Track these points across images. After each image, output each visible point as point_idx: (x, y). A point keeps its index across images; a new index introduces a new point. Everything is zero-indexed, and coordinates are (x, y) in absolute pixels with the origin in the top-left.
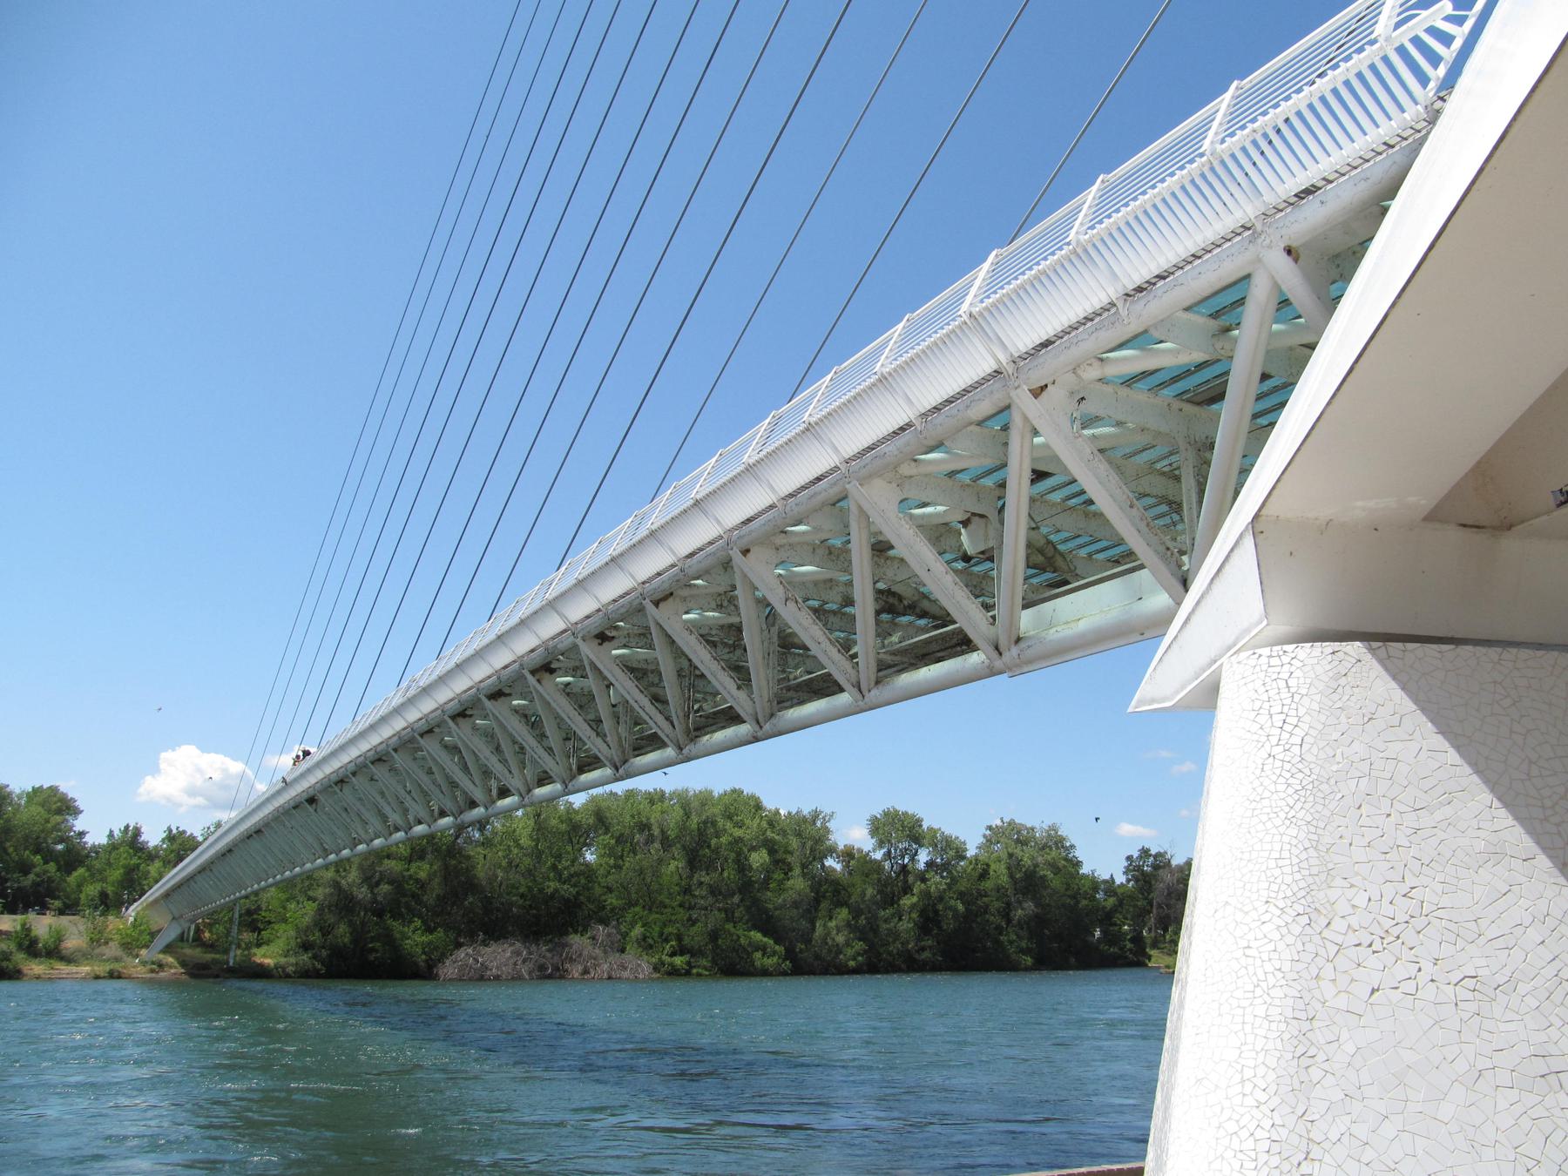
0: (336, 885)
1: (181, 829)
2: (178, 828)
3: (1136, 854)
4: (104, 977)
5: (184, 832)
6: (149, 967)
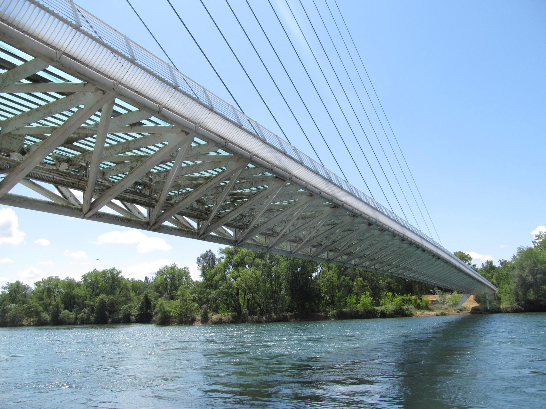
0: (521, 276)
1: (504, 260)
2: (503, 260)
3: (208, 251)
4: (439, 315)
5: (506, 261)
6: (456, 311)
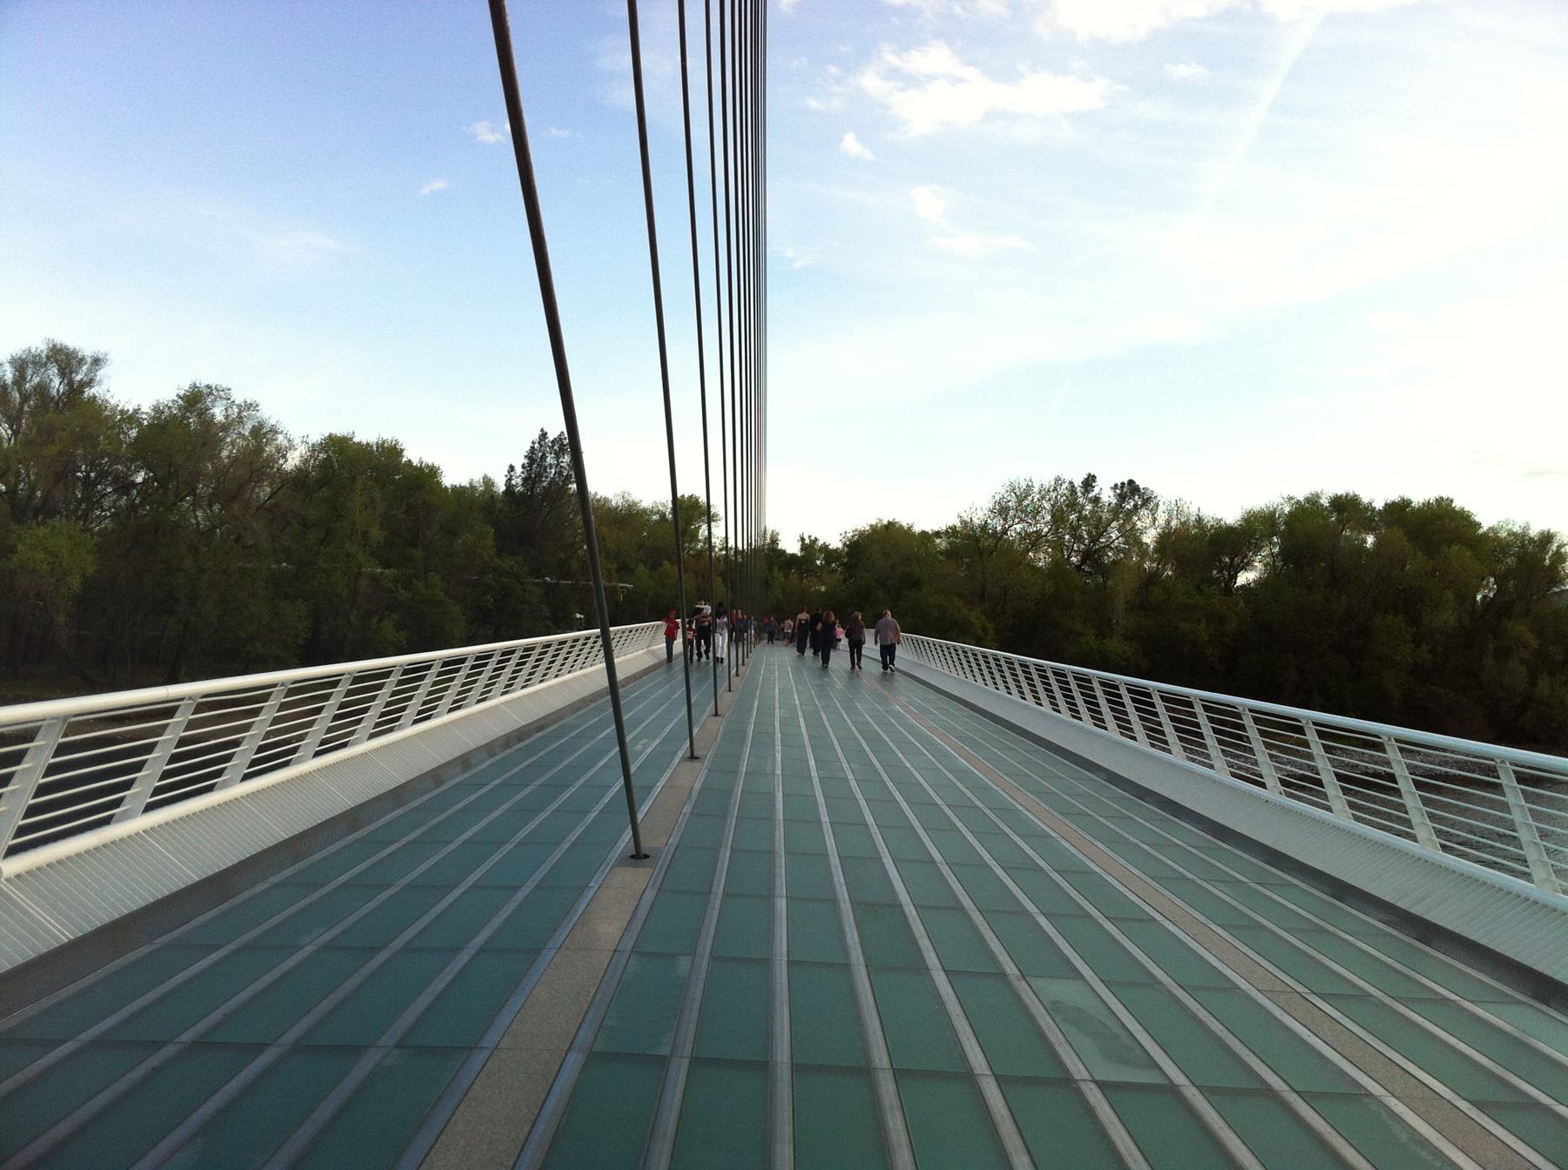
2: (810, 537)
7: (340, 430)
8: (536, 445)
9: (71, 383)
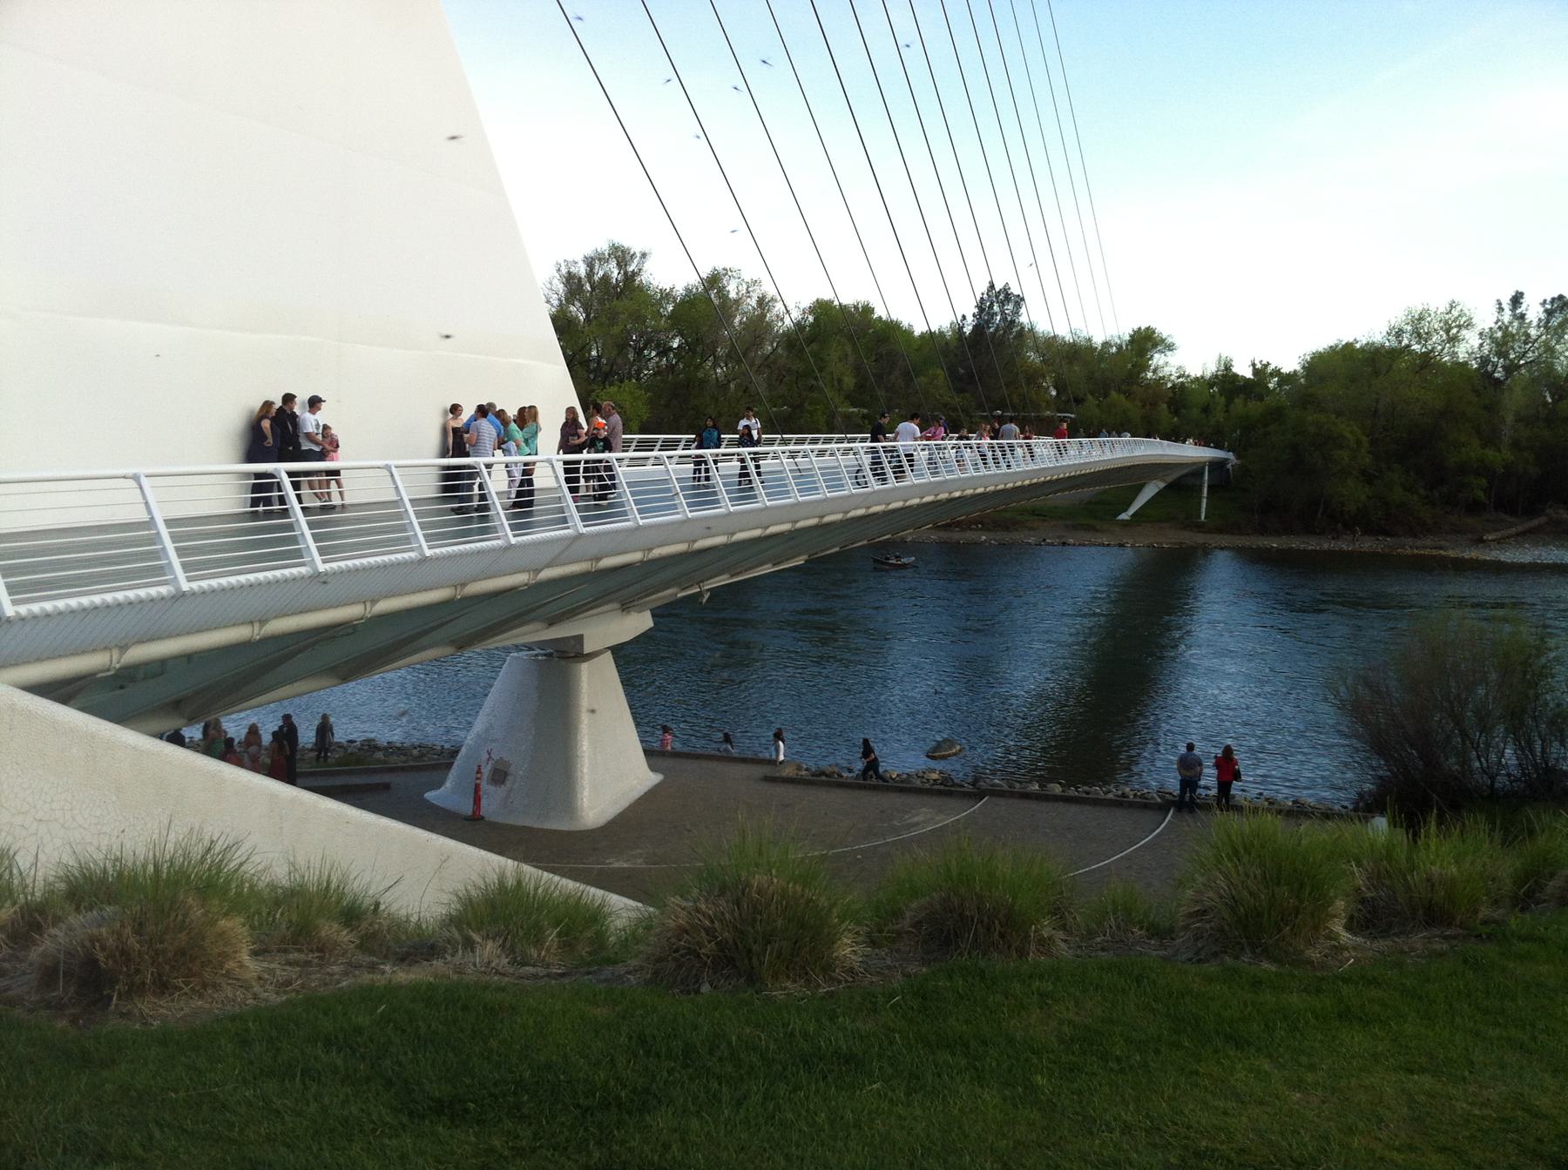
7: (287, 392)
8: (985, 296)
9: (626, 273)
